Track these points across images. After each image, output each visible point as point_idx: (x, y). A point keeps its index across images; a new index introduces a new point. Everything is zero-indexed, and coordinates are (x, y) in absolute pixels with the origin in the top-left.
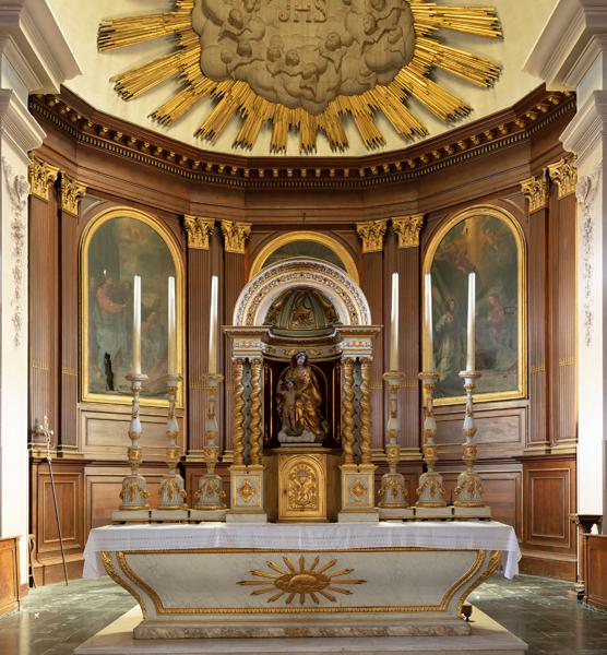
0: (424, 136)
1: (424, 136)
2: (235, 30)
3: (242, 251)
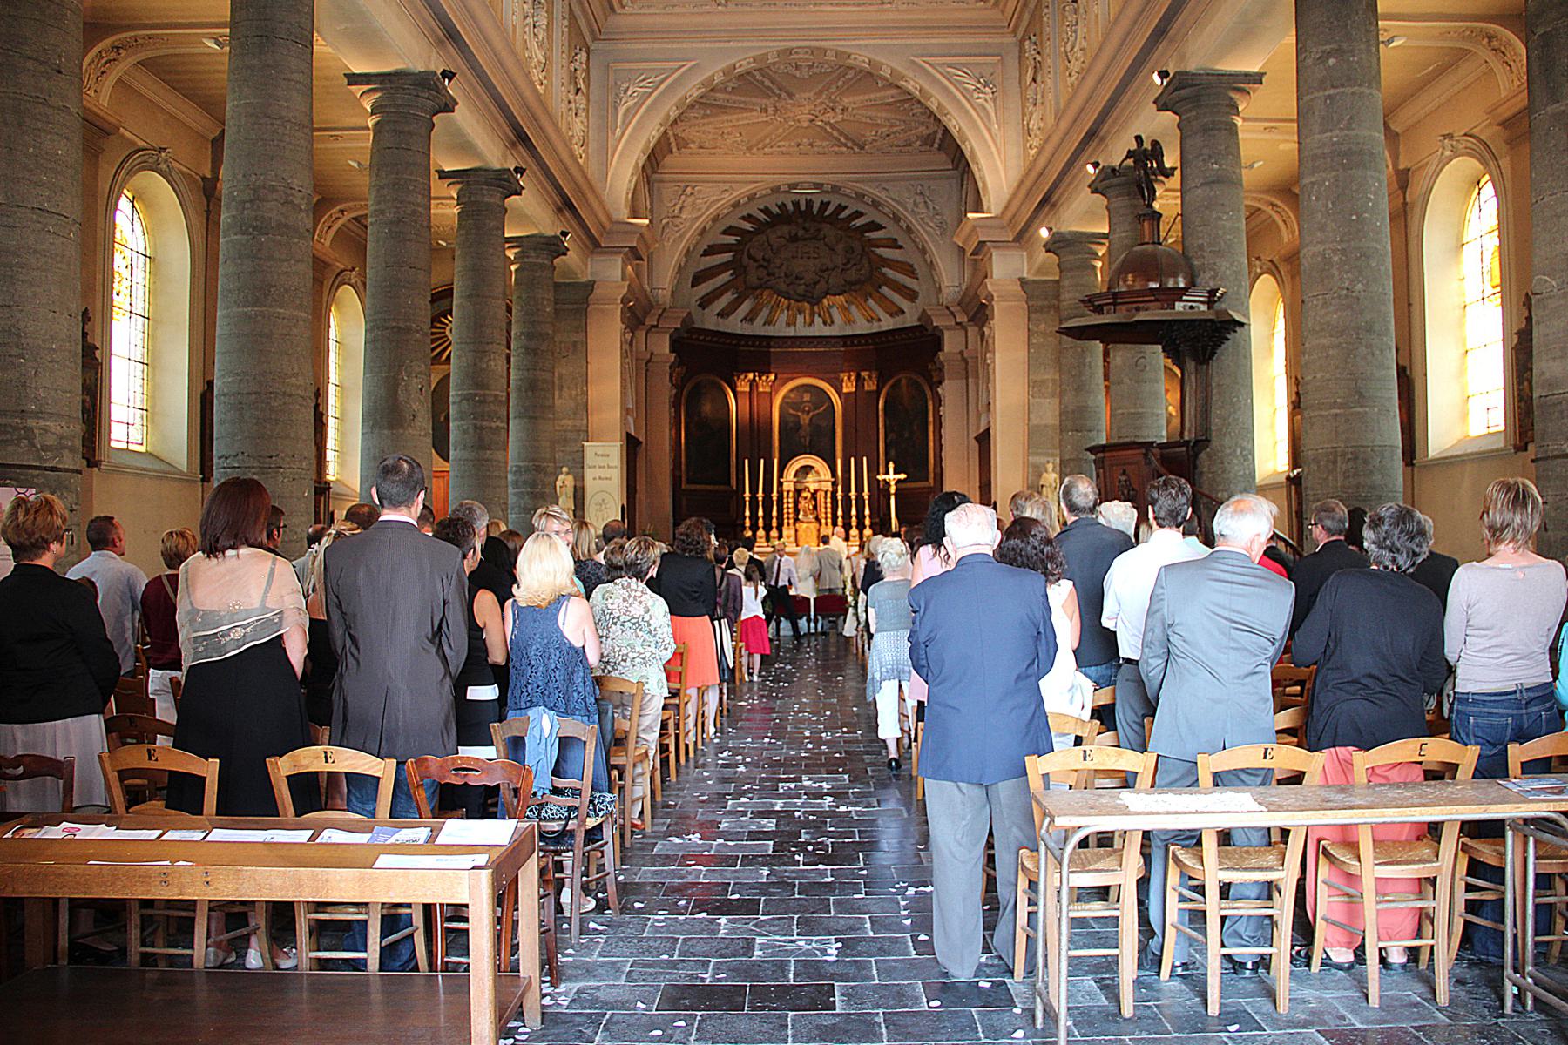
2: (765, 264)
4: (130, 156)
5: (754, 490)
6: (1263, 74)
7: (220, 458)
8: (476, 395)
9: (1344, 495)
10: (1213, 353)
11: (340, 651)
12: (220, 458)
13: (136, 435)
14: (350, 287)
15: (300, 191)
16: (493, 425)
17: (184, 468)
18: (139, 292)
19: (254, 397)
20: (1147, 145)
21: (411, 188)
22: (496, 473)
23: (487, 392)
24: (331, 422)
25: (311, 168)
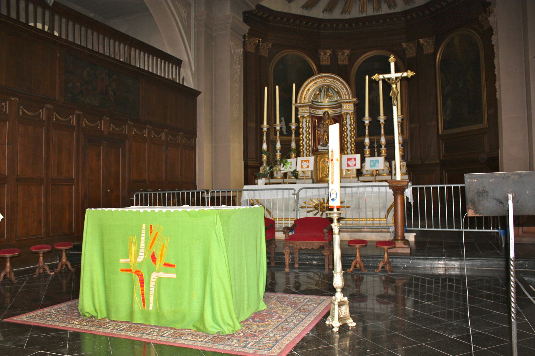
0: (394, 8)
1: (394, 8)
3: (267, 56)
5: (272, 120)
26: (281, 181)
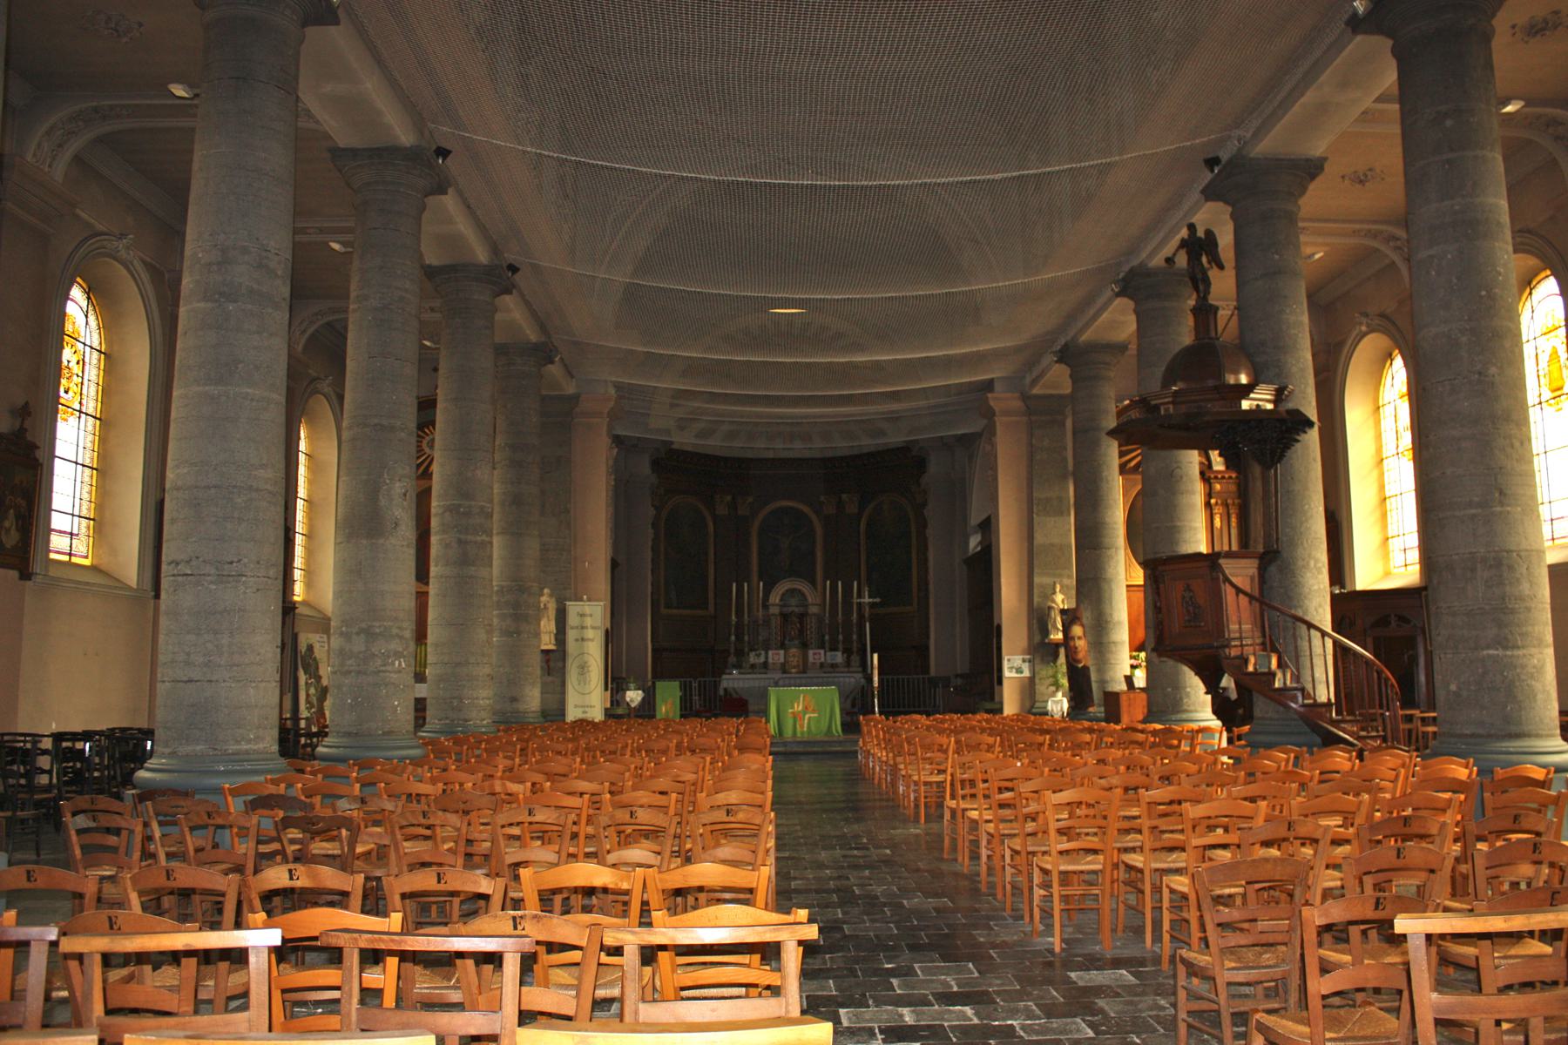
4: (86, 239)
6: (1325, 159)
7: (170, 564)
8: (460, 506)
9: (1487, 607)
10: (1282, 456)
11: (91, 312)
12: (170, 564)
13: (81, 546)
14: (322, 397)
15: (277, 254)
16: (479, 539)
17: (134, 583)
18: (91, 391)
19: (213, 491)
20: (1200, 233)
21: (399, 272)
22: (481, 592)
23: (473, 503)
24: (299, 539)
25: (256, 706)
26: (750, 671)
